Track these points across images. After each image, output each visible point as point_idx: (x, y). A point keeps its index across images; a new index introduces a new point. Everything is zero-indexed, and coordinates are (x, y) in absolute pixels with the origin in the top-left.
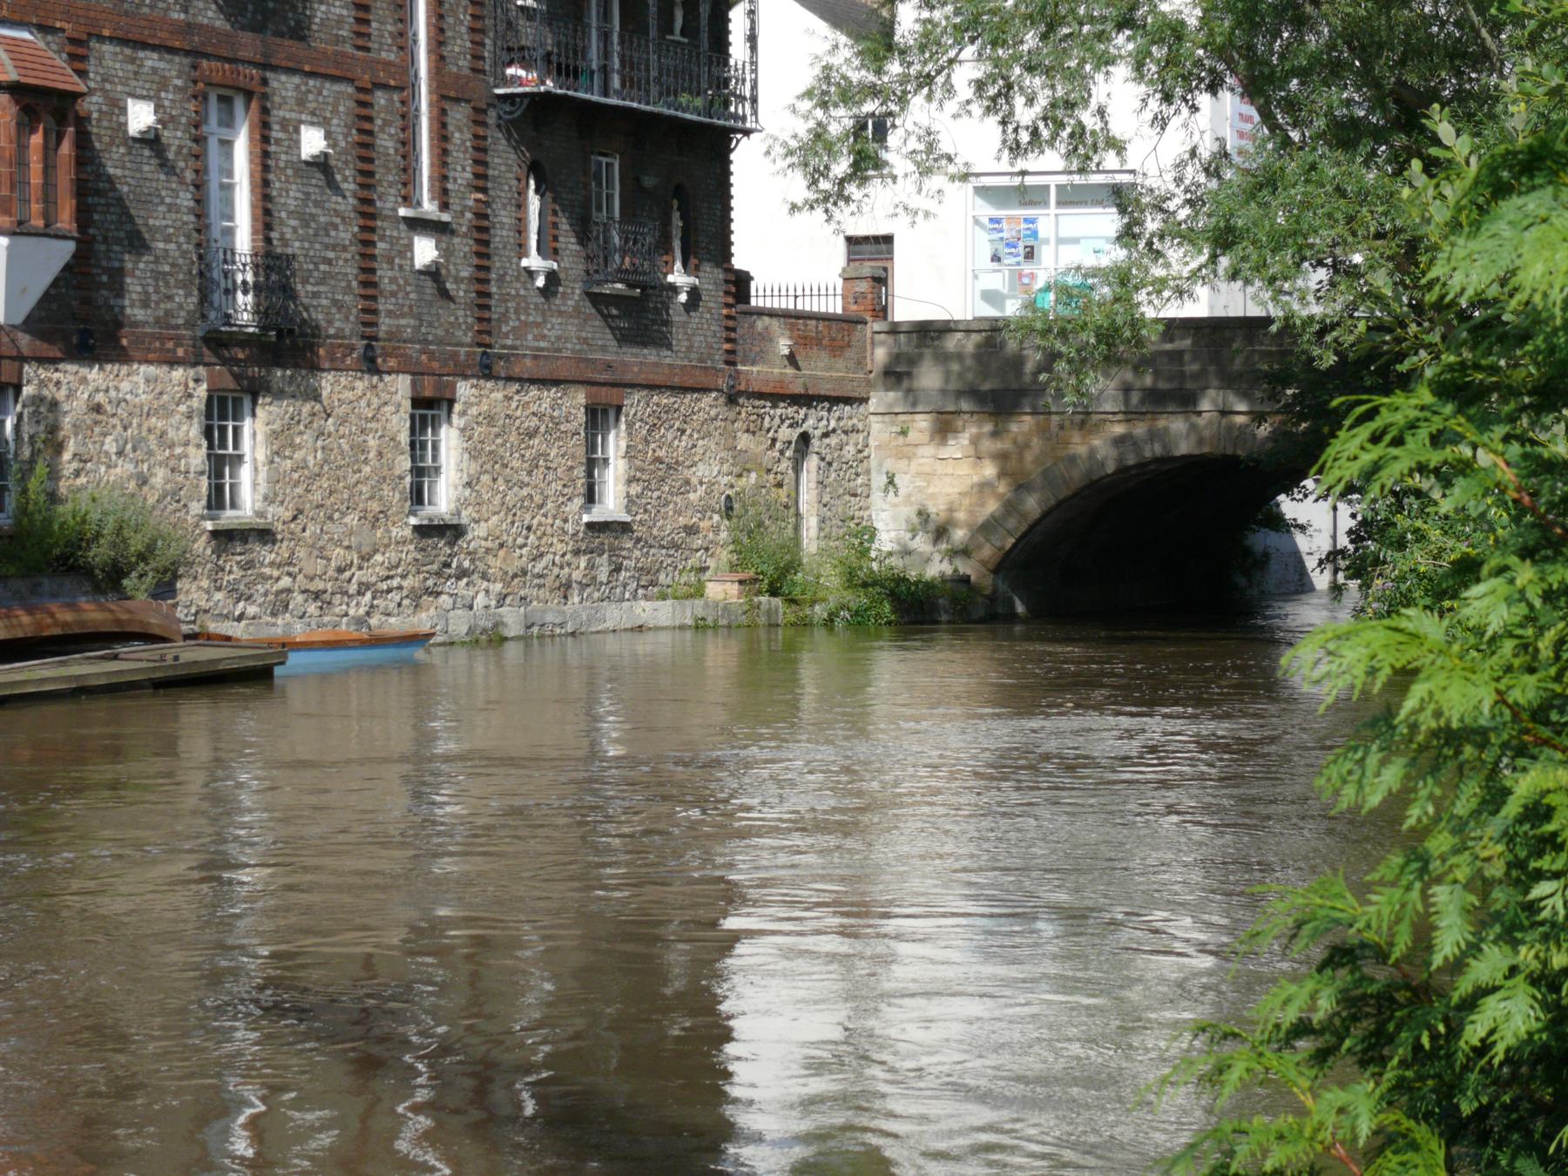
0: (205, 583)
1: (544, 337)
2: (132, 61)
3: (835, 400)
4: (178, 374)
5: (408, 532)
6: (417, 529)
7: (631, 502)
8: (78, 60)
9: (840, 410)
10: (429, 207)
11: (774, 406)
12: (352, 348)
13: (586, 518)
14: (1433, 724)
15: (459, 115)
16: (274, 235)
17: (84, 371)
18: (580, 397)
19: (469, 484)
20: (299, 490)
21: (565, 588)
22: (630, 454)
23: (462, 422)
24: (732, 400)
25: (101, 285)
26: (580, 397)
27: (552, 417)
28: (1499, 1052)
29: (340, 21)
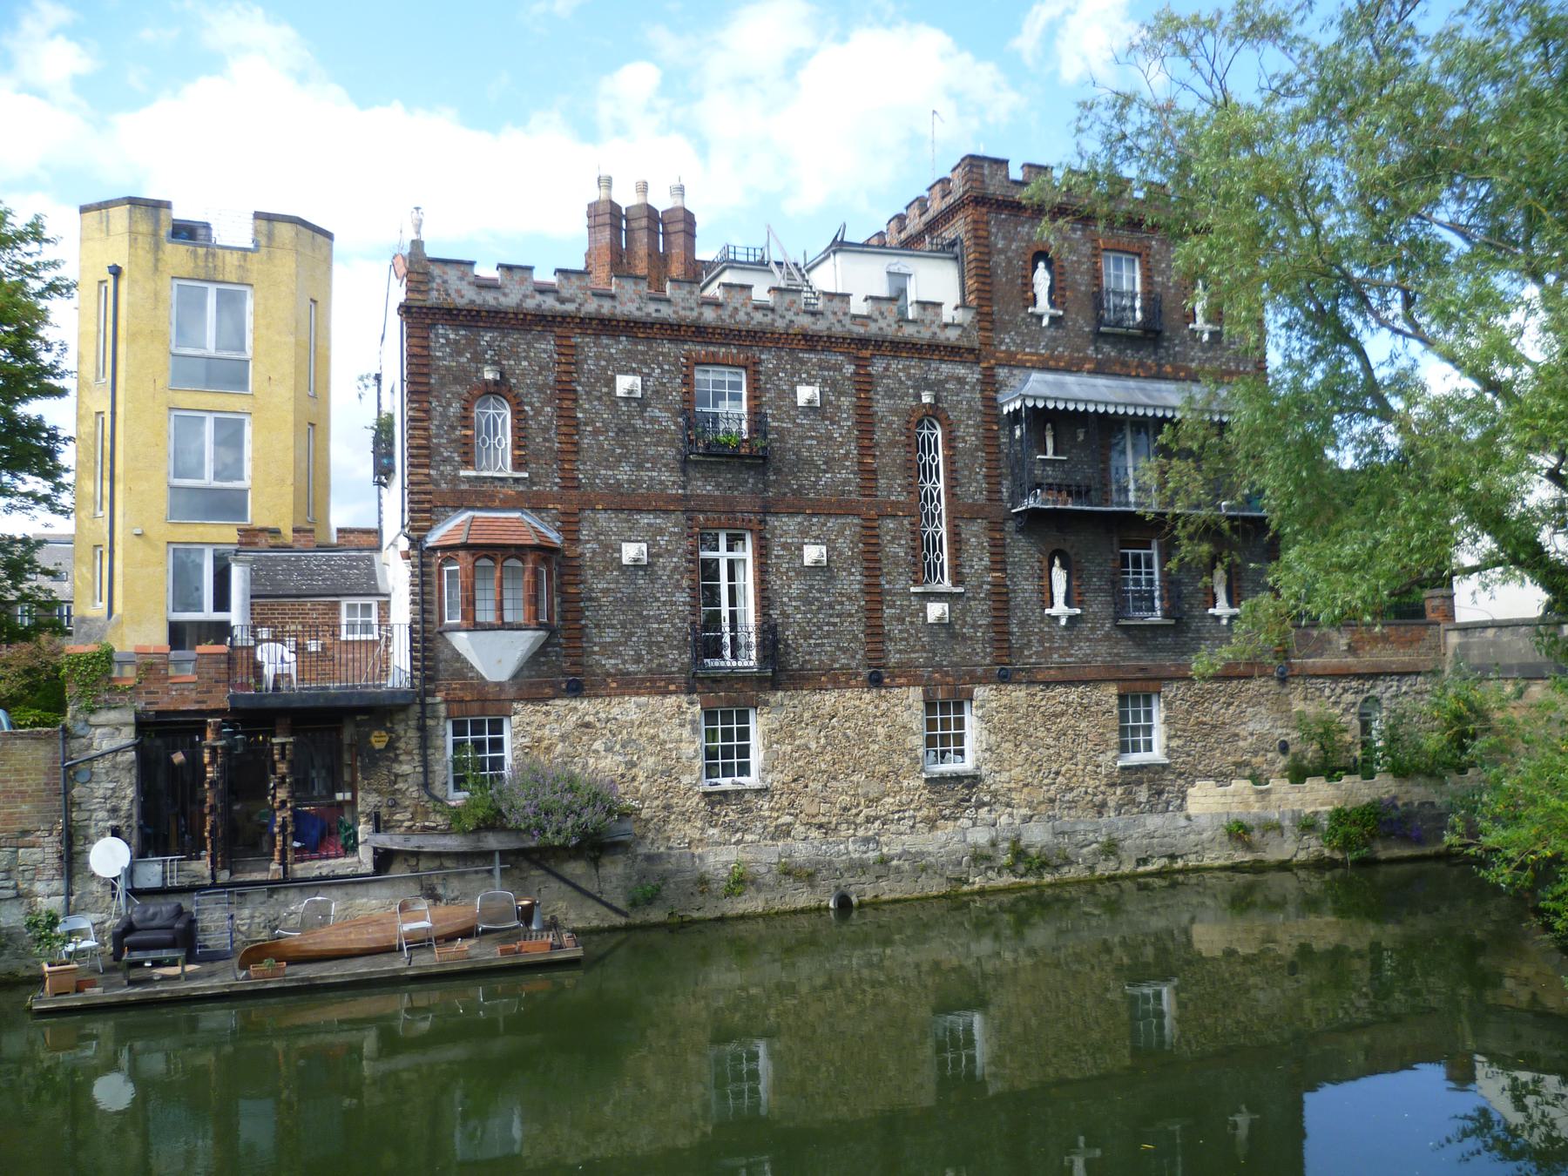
0: (699, 824)
1: (1071, 656)
2: (628, 521)
3: (1402, 675)
4: (671, 700)
5: (922, 783)
6: (927, 780)
7: (1170, 752)
8: (570, 527)
9: (1409, 681)
10: (946, 585)
11: (1337, 682)
12: (859, 674)
13: (1119, 764)
14: (423, 905)
15: (976, 534)
16: (775, 613)
17: (574, 703)
18: (1113, 689)
19: (989, 749)
20: (867, 987)
21: (1101, 808)
22: (1168, 721)
23: (980, 713)
24: (1283, 680)
25: (595, 653)
26: (1113, 689)
27: (1080, 704)
28: (659, 868)
29: (846, 482)
